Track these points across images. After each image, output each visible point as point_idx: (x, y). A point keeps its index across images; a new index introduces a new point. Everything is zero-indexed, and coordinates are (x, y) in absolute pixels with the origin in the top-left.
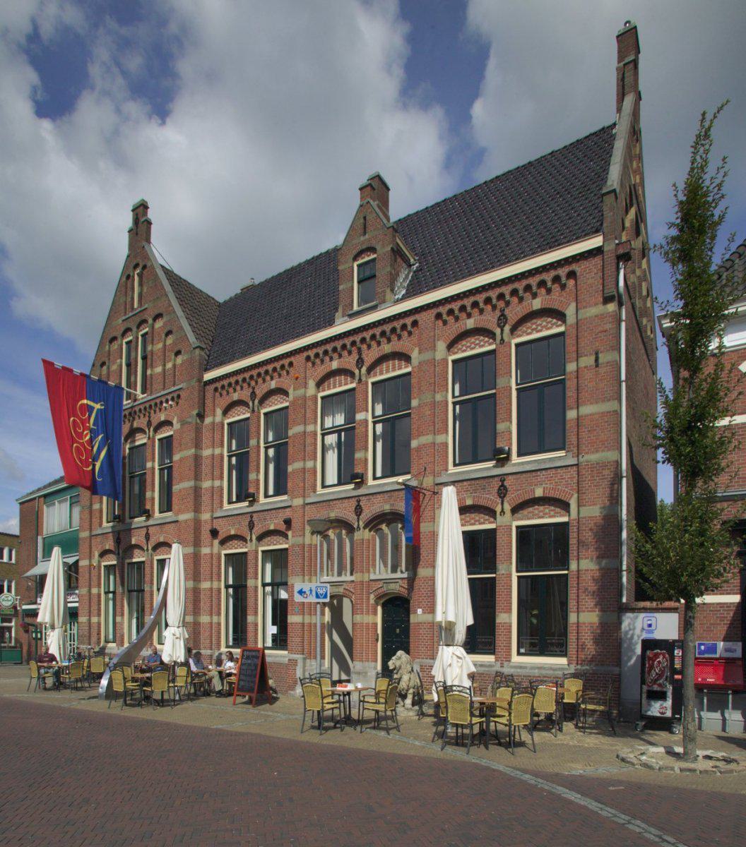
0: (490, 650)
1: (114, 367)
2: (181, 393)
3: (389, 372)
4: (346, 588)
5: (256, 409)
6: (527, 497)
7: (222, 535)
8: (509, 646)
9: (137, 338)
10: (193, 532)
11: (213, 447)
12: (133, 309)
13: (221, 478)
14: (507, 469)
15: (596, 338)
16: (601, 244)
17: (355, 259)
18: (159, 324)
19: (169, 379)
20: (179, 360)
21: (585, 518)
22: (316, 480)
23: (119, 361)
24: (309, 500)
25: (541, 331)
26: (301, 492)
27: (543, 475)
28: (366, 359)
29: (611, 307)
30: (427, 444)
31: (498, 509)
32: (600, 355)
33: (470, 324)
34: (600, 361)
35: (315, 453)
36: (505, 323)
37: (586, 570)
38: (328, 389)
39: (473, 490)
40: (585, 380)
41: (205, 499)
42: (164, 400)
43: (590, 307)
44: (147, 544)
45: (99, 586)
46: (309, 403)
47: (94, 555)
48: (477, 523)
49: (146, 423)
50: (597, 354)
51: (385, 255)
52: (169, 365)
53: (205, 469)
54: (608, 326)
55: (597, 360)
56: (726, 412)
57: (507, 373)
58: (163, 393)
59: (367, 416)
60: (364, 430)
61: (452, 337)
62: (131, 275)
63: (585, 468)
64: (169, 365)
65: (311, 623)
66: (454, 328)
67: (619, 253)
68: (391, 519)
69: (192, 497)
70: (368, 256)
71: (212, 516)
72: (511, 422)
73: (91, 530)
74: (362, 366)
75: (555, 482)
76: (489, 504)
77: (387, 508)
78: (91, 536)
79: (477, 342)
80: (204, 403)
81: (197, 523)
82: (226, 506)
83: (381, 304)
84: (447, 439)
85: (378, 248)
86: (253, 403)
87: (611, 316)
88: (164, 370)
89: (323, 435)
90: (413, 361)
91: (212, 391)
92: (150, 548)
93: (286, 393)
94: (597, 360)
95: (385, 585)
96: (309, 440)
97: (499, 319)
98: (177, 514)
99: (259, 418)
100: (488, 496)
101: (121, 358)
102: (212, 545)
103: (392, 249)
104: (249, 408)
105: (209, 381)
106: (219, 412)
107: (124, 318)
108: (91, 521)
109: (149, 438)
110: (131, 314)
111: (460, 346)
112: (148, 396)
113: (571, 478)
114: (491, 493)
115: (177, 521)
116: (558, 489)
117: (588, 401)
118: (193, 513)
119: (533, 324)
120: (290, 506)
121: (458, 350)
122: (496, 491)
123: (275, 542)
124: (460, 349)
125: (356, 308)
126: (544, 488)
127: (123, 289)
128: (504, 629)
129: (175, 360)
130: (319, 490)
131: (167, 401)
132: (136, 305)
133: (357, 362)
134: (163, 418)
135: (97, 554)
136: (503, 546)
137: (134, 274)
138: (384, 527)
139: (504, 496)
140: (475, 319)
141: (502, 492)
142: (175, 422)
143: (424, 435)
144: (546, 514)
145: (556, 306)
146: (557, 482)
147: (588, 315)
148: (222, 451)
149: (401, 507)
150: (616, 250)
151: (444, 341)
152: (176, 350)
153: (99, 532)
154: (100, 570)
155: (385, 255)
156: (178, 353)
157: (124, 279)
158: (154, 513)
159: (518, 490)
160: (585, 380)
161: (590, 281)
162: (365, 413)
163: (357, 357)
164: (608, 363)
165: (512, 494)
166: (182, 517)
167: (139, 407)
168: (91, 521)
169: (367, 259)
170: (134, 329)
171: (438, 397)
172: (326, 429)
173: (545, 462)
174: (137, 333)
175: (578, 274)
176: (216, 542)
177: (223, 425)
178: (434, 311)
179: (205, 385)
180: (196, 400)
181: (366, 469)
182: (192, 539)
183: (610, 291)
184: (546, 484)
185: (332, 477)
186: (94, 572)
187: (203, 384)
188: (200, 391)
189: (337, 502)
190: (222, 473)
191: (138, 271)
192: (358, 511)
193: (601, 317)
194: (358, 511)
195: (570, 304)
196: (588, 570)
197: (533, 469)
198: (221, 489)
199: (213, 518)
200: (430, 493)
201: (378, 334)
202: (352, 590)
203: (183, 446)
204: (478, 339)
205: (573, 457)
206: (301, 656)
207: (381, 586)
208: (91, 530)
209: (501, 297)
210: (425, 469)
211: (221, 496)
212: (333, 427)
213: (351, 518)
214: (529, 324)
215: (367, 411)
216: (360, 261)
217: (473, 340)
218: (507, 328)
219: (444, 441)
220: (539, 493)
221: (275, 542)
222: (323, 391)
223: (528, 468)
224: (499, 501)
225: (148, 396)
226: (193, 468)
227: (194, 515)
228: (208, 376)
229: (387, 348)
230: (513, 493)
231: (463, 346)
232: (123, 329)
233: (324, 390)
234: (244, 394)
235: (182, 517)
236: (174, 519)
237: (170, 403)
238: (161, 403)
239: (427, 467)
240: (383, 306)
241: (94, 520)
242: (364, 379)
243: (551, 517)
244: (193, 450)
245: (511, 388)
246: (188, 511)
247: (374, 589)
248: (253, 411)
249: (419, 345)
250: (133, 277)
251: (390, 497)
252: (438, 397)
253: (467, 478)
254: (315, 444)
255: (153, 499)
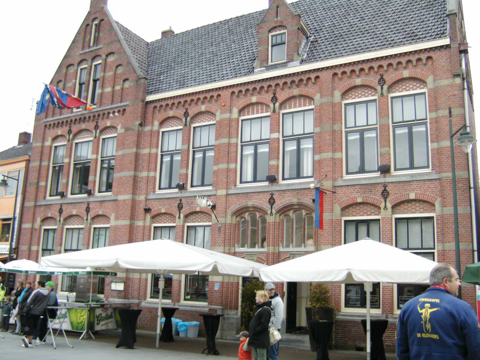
0: (375, 305)
1: (69, 85)
2: (126, 109)
3: (291, 108)
4: (259, 256)
5: (188, 124)
6: (403, 199)
7: (154, 212)
8: (392, 307)
9: (91, 67)
10: (130, 209)
11: (150, 148)
12: (89, 47)
13: (155, 170)
14: (388, 179)
15: (449, 99)
16: (449, 43)
17: (270, 31)
18: (111, 59)
19: (117, 98)
20: (127, 85)
21: (447, 215)
22: (236, 178)
23: (74, 81)
24: (231, 192)
25: (409, 90)
26: (225, 185)
27: (415, 184)
28: (279, 97)
29: (458, 80)
30: (327, 159)
31: (382, 206)
32: (452, 110)
33: (406, 74)
34: (453, 114)
35: (236, 158)
36: (98, 128)
37: (449, 250)
38: (294, 107)
39: (363, 192)
40: (442, 125)
41: (142, 185)
42: (111, 112)
43: (443, 79)
44: (87, 215)
45: (38, 245)
46: (234, 124)
47: (36, 221)
48: (365, 215)
49: (93, 126)
50: (450, 109)
51: (293, 32)
52: (118, 88)
53: (143, 163)
54: (456, 92)
55: (450, 112)
56: (195, 326)
57: (386, 115)
58: (110, 106)
59: (279, 135)
60: (277, 145)
61: (345, 89)
62: (91, 24)
63: (445, 182)
64: (118, 88)
65: (229, 282)
66: (347, 83)
67: (461, 49)
68: (296, 208)
69: (131, 183)
70: (280, 30)
71: (146, 198)
72: (390, 147)
73: (36, 200)
74: (276, 102)
75: (424, 190)
76: (375, 202)
77: (295, 201)
78: (36, 206)
79: (363, 93)
80: (145, 117)
81: (134, 204)
82: (158, 191)
83: (289, 62)
84: (342, 156)
85: (288, 27)
86: (186, 120)
87: (458, 86)
88: (113, 91)
89: (394, 128)
90: (315, 102)
91: (152, 109)
92: (89, 218)
93: (213, 114)
94: (450, 112)
95: (291, 255)
96: (233, 149)
97: (379, 81)
98: (117, 194)
99: (190, 130)
100: (374, 197)
101: (76, 79)
102: (145, 219)
103: (298, 28)
104: (182, 122)
105: (150, 101)
106: (156, 123)
107: (81, 52)
108: (37, 194)
109: (95, 137)
110: (87, 50)
111: (350, 95)
112: (97, 107)
113: (435, 187)
114: (376, 195)
115: (117, 200)
116: (426, 194)
117: (445, 138)
118: (131, 195)
119: (403, 86)
120: (215, 195)
121: (396, 90)
122: (380, 193)
123: (199, 220)
124: (351, 97)
125: (270, 63)
126: (416, 193)
127: (83, 34)
128: (388, 290)
129: (123, 85)
130: (239, 185)
131: (114, 112)
132: (92, 44)
133: (95, 126)
134: (109, 124)
135: (39, 220)
136: (386, 232)
137: (92, 24)
138: (291, 213)
139: (386, 198)
140: (362, 80)
141: (385, 194)
142: (119, 127)
143: (325, 152)
144: (417, 210)
145: (419, 76)
146: (425, 190)
147: (442, 84)
148: (157, 151)
149: (307, 200)
150: (459, 48)
151: (339, 91)
152: (124, 77)
153: (44, 203)
154: (40, 232)
155: (293, 32)
156: (125, 80)
157: (84, 26)
158: (94, 192)
159: (397, 194)
160: (442, 125)
161: (442, 64)
162: (277, 133)
163: (272, 96)
164: (458, 115)
165: (392, 196)
166: (121, 197)
167: (103, 112)
168: (37, 194)
169: (278, 32)
170: (90, 61)
171: (336, 127)
172: (194, 155)
173: (282, 230)
174: (92, 63)
175: (434, 59)
176: (148, 216)
177: (159, 132)
178: (332, 72)
179: (146, 104)
180: (140, 114)
181: (278, 172)
182: (129, 215)
183: (458, 72)
184: (418, 190)
185: (249, 174)
186: (36, 234)
187: (145, 103)
188: (142, 108)
189: (254, 194)
190: (156, 167)
191: (96, 22)
192: (272, 201)
193: (452, 86)
194: (272, 201)
195: (429, 76)
196: (450, 250)
197: (408, 180)
198: (155, 178)
199: (147, 200)
200: (329, 192)
201: (289, 82)
202: (264, 258)
203: (125, 146)
204: (412, 84)
205: (436, 174)
206: (221, 307)
207: (288, 256)
208: (36, 200)
209: (381, 67)
210: (326, 175)
211: (155, 184)
212: (251, 141)
213: (266, 206)
214: (400, 86)
215: (279, 132)
216: (274, 33)
217: (360, 92)
218: (385, 87)
219: (340, 157)
220: (412, 196)
221: (199, 220)
222: (243, 116)
223: (404, 179)
224: (383, 200)
225: (97, 107)
226: (134, 163)
227: (132, 196)
228: (150, 98)
229: (296, 91)
230: (393, 196)
231: (352, 95)
232: (79, 60)
233: (244, 115)
234: (180, 112)
235: (121, 197)
236: (113, 198)
237: (116, 114)
238: (109, 113)
239: (328, 174)
240: (291, 64)
241: (39, 193)
242: (277, 110)
243: (421, 212)
244: (134, 150)
245: (389, 125)
246: (127, 193)
247: (282, 259)
248: (186, 125)
249: (321, 93)
250: (92, 26)
251: (298, 194)
252: (336, 127)
253: (358, 183)
254: (237, 152)
255: (95, 182)
